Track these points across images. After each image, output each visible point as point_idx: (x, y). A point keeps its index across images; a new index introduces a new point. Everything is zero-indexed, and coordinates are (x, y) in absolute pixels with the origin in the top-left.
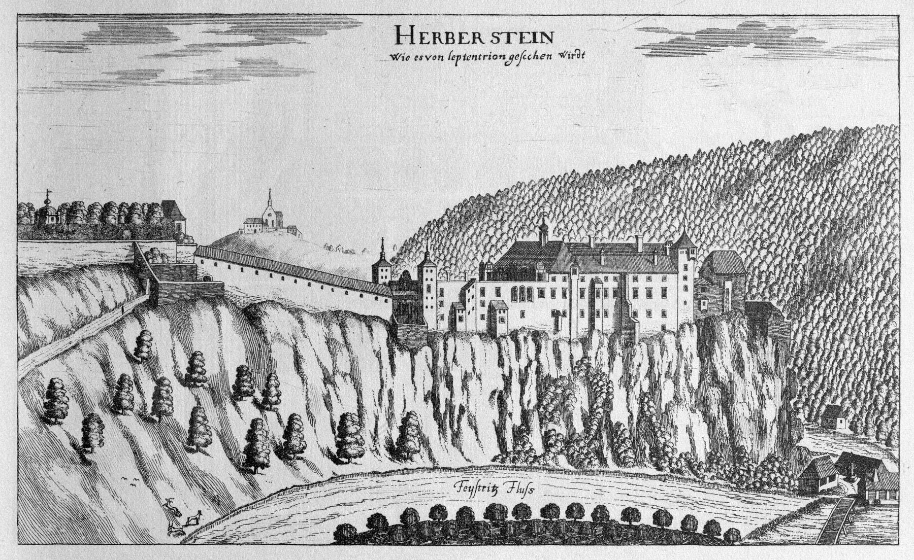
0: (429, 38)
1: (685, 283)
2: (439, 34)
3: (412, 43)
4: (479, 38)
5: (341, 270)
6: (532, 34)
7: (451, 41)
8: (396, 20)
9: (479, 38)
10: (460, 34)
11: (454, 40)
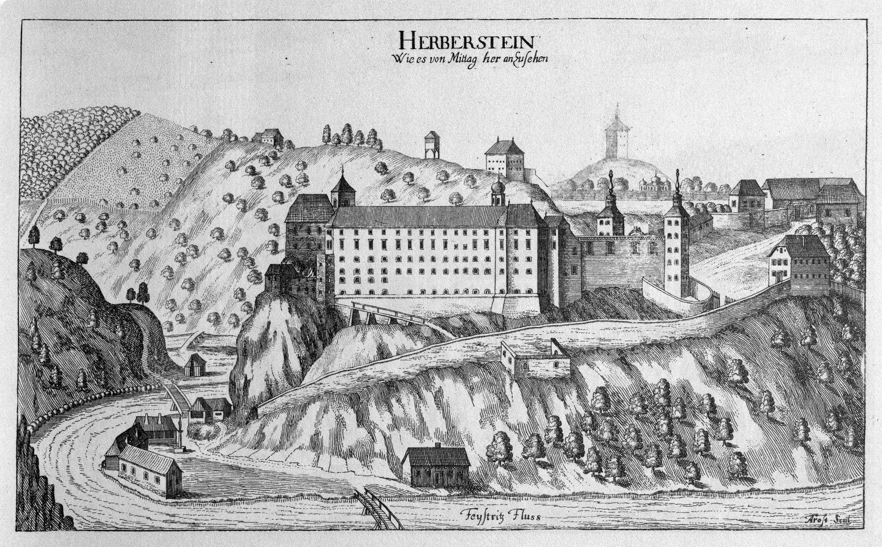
0: (427, 43)
1: (357, 265)
2: (437, 39)
3: (413, 48)
4: (470, 43)
5: (552, 264)
6: (513, 38)
7: (445, 45)
8: (402, 26)
9: (470, 43)
10: (453, 38)
11: (448, 44)
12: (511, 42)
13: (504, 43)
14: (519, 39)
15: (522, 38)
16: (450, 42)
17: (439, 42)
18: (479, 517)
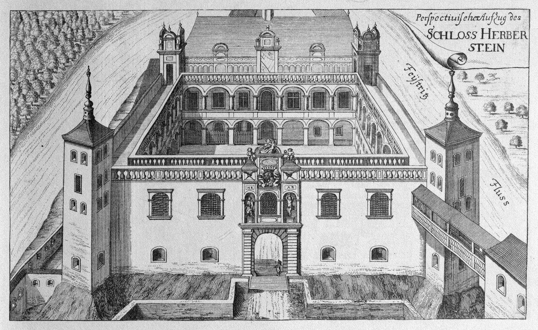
10: (514, 32)
12: (483, 48)
13: (487, 48)
14: (496, 46)
15: (498, 45)
16: (512, 35)
17: (506, 35)
18: (414, 79)
